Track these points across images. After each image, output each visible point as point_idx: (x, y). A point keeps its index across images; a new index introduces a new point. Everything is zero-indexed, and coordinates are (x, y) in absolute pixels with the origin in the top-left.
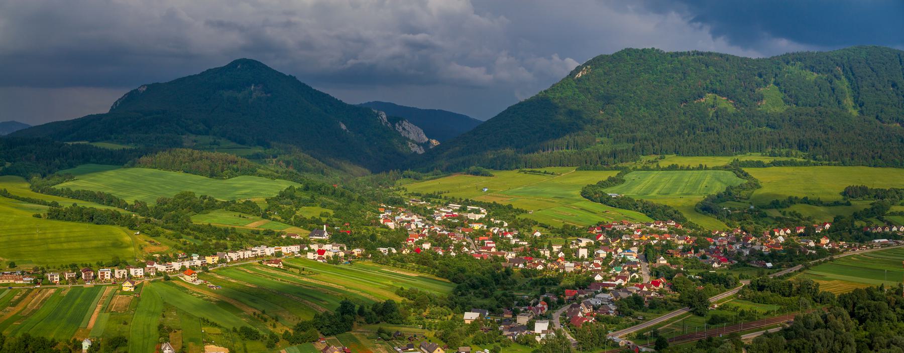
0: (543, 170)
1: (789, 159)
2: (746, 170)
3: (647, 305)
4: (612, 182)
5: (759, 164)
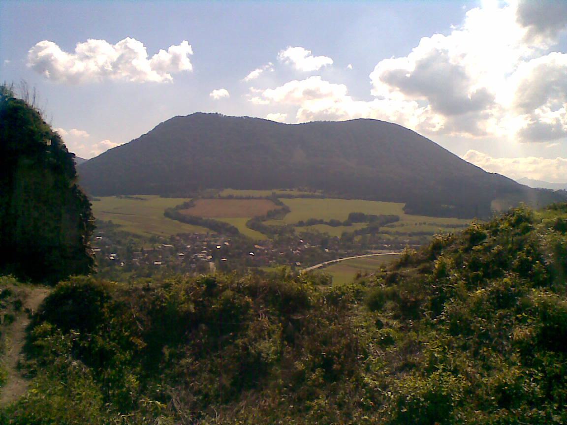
0: (134, 196)
1: (310, 194)
2: (281, 200)
3: (389, 304)
4: (186, 206)
5: (290, 197)
